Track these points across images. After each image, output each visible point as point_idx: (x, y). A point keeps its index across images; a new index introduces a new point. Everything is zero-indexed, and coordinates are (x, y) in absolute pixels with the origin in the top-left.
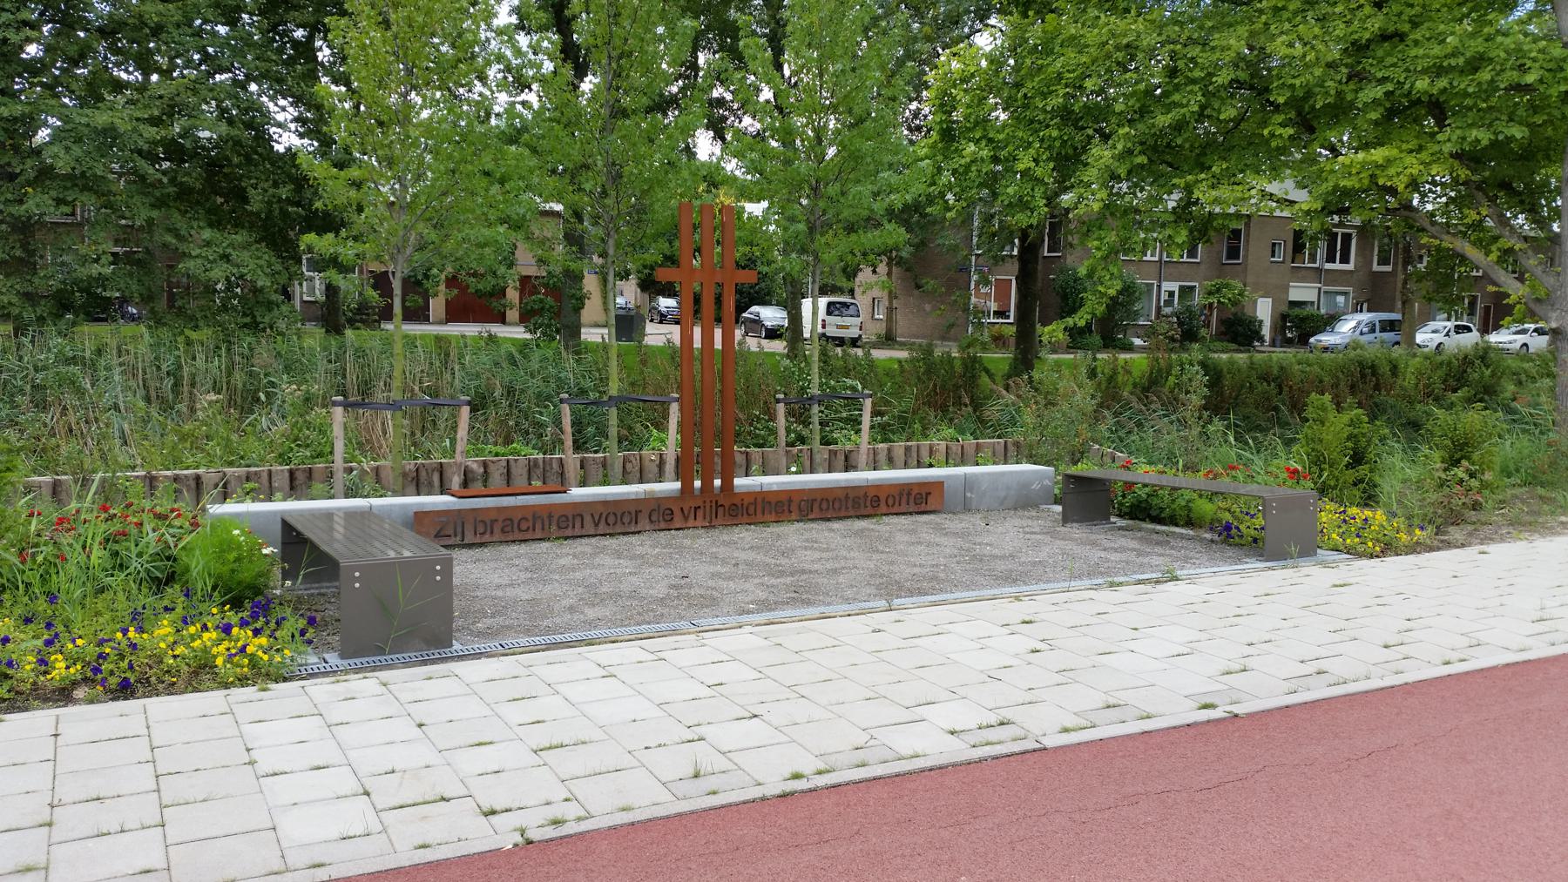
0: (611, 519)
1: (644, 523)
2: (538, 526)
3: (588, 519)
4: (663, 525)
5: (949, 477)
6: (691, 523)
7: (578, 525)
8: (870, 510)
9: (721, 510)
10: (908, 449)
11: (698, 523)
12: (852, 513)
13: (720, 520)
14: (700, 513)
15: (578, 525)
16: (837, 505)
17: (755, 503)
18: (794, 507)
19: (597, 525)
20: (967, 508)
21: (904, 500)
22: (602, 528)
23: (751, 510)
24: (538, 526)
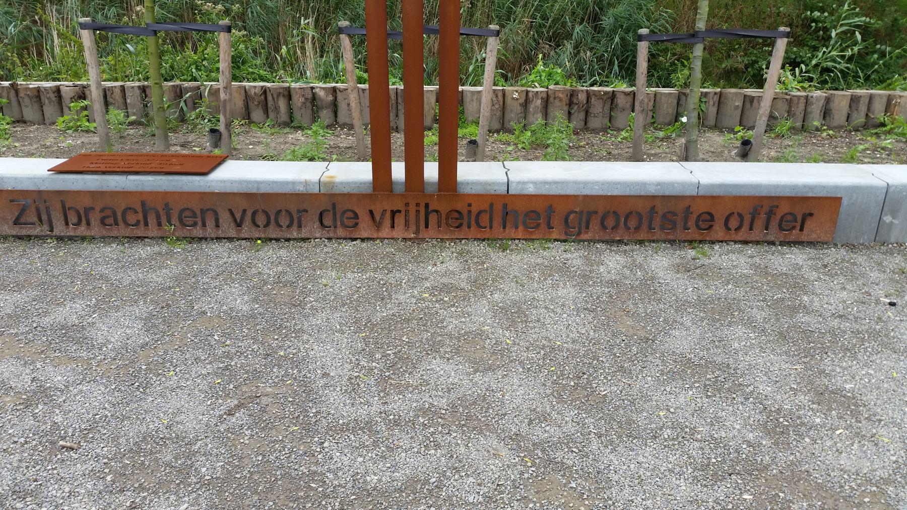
0: (261, 219)
1: (311, 227)
2: (152, 220)
3: (225, 217)
4: (341, 232)
5: (855, 189)
6: (385, 232)
7: (210, 223)
8: (692, 233)
9: (433, 218)
10: (854, 100)
11: (395, 234)
12: (658, 234)
13: (432, 231)
14: (400, 220)
15: (210, 223)
16: (632, 223)
17: (550, 210)
18: (556, 221)
19: (239, 225)
20: (880, 241)
21: (759, 223)
22: (247, 230)
23: (485, 220)
24: (152, 220)
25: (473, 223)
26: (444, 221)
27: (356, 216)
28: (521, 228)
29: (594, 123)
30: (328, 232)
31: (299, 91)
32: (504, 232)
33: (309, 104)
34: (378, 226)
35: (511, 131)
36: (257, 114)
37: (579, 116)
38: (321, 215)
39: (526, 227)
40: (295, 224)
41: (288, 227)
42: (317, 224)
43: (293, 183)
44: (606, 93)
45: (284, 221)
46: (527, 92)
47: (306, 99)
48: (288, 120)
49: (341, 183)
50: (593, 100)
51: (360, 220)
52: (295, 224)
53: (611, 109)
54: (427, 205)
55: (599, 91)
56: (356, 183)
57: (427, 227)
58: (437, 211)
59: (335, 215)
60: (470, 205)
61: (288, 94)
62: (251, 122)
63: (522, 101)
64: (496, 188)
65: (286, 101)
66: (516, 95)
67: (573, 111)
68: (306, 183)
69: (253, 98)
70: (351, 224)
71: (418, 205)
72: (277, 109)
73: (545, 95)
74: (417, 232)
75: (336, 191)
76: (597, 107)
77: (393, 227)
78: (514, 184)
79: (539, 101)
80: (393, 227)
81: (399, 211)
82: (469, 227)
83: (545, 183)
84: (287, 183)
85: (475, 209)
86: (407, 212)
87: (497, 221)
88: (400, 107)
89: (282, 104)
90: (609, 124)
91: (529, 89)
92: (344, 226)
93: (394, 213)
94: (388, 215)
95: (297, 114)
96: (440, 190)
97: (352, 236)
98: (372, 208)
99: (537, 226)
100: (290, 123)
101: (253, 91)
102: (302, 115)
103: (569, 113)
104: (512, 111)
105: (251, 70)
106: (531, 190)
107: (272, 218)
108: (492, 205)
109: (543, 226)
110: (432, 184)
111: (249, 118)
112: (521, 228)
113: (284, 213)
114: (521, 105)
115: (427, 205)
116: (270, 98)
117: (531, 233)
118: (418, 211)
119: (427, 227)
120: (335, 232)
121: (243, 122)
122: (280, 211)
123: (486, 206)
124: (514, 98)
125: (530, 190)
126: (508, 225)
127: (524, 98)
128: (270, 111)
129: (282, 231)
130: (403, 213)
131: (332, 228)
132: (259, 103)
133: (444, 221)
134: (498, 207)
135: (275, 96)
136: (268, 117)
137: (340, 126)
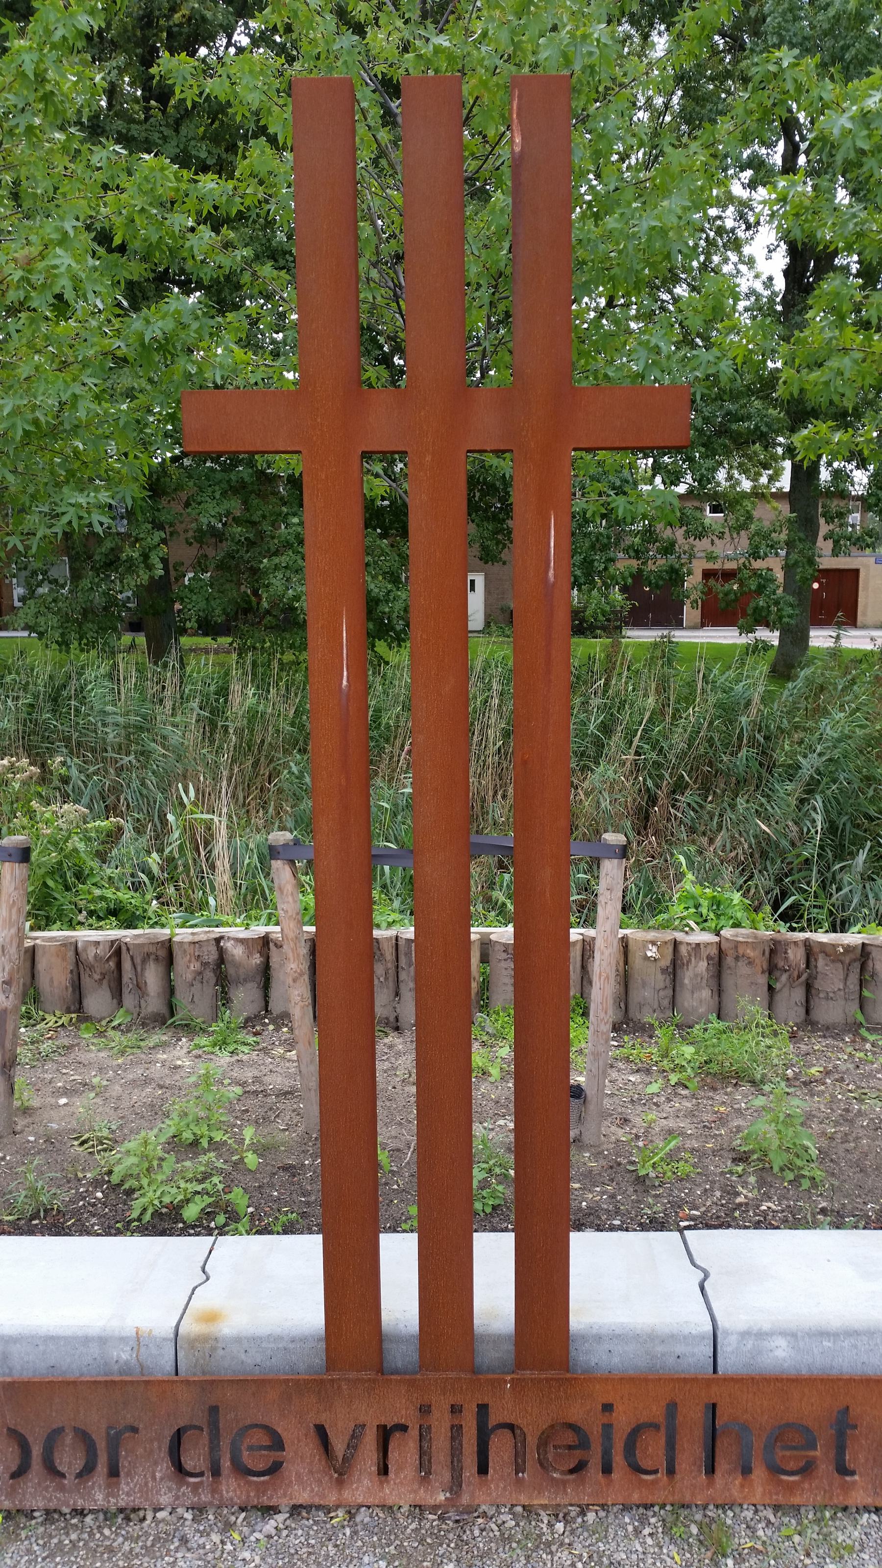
1: (146, 1477)
4: (231, 1488)
6: (362, 1487)
9: (501, 1448)
14: (404, 1452)
23: (653, 1450)
25: (618, 1459)
26: (532, 1455)
27: (278, 1444)
28: (759, 1473)
29: (829, 1011)
30: (195, 1488)
31: (190, 950)
32: (711, 1483)
33: (209, 975)
34: (341, 1470)
35: (647, 1030)
36: (97, 1001)
37: (791, 999)
38: (178, 1436)
39: (775, 1470)
40: (102, 1468)
41: (80, 1475)
42: (164, 1468)
43: (103, 1340)
44: (848, 949)
45: (69, 1460)
46: (676, 944)
47: (205, 965)
48: (164, 1010)
49: (238, 1340)
50: (821, 963)
51: (288, 1454)
52: (102, 1468)
53: (862, 983)
54: (483, 1409)
55: (834, 946)
56: (280, 1338)
57: (483, 1469)
58: (511, 1427)
59: (214, 1446)
60: (608, 1408)
61: (167, 954)
62: (84, 1018)
63: (666, 962)
64: (680, 1349)
65: (161, 969)
66: (652, 952)
67: (778, 986)
68: (139, 1340)
69: (91, 968)
70: (261, 1466)
71: (455, 1410)
72: (140, 987)
73: (714, 951)
74: (456, 1485)
75: (229, 1364)
76: (831, 979)
77: (384, 1470)
78: (733, 1339)
79: (703, 965)
80: (384, 1470)
81: (404, 1428)
82: (607, 1470)
83: (823, 1334)
84: (86, 1340)
85: (623, 1421)
86: (424, 1434)
87: (690, 1452)
88: (403, 976)
89: (152, 977)
90: (860, 1017)
91: (679, 936)
92: (242, 1471)
93: (385, 1435)
94: (370, 1440)
95: (182, 998)
96: (520, 1364)
97: (265, 1501)
98: (324, 1418)
99: (807, 1469)
100: (167, 1017)
101: (91, 953)
102: (194, 1001)
103: (770, 988)
104: (644, 984)
105: (97, 892)
106: (780, 1355)
107: (36, 1451)
108: (672, 1408)
109: (825, 1468)
110: (496, 1339)
111: (80, 1009)
112: (759, 1473)
113: (69, 1438)
114: (664, 971)
115: (483, 1409)
116: (127, 965)
117: (791, 1488)
118: (456, 1431)
119: (483, 1469)
120: (214, 1491)
121: (65, 1020)
122: (60, 1431)
123: (656, 1412)
124: (647, 958)
125: (780, 1354)
126: (722, 1465)
127: (669, 957)
128: (125, 991)
129: (62, 1488)
130: (414, 1432)
131: (208, 1478)
132: (103, 975)
133: (532, 1455)
134: (693, 1416)
135: (138, 961)
136: (120, 1004)
137: (273, 1021)
